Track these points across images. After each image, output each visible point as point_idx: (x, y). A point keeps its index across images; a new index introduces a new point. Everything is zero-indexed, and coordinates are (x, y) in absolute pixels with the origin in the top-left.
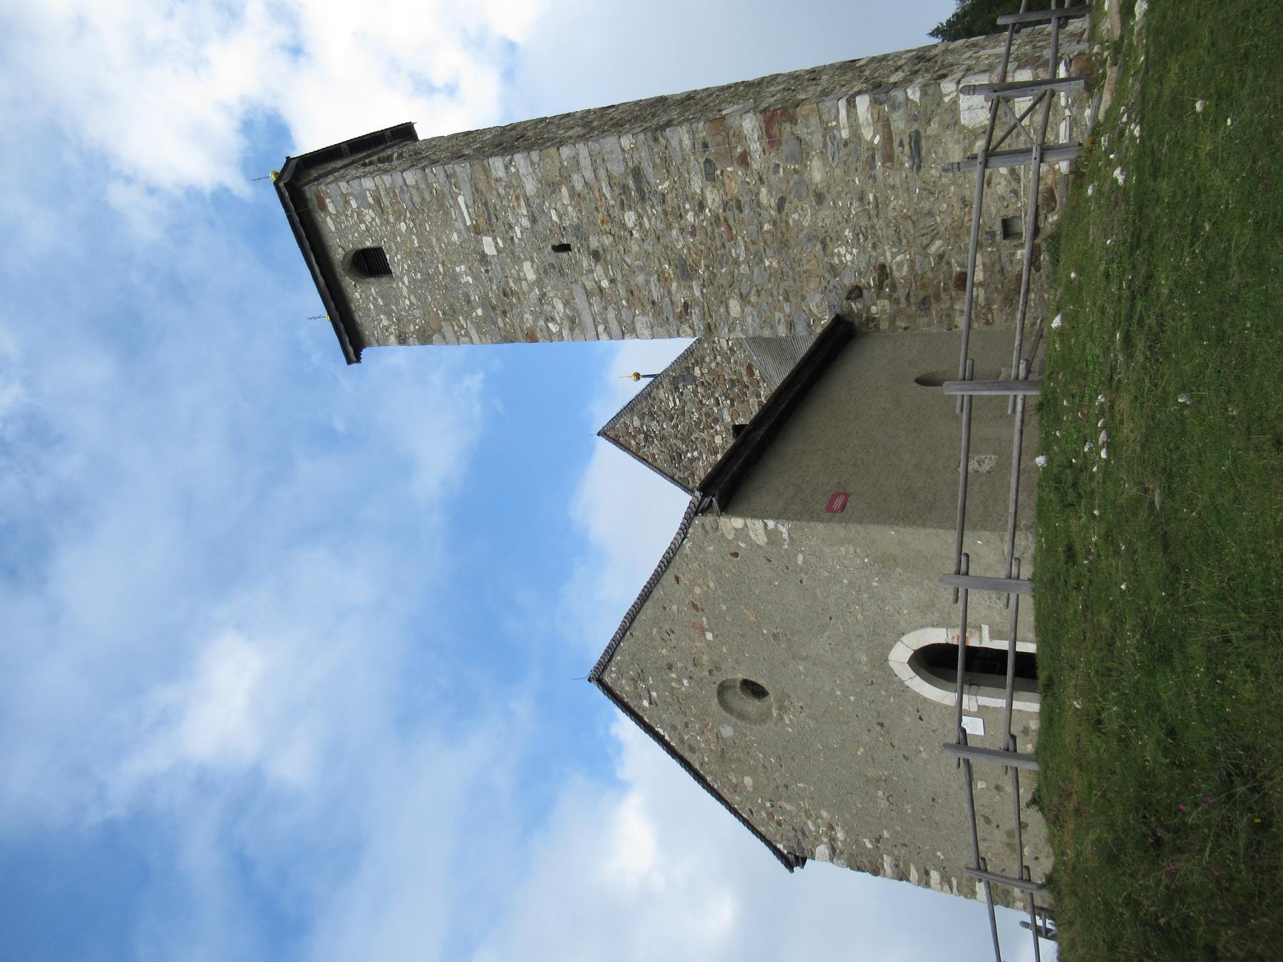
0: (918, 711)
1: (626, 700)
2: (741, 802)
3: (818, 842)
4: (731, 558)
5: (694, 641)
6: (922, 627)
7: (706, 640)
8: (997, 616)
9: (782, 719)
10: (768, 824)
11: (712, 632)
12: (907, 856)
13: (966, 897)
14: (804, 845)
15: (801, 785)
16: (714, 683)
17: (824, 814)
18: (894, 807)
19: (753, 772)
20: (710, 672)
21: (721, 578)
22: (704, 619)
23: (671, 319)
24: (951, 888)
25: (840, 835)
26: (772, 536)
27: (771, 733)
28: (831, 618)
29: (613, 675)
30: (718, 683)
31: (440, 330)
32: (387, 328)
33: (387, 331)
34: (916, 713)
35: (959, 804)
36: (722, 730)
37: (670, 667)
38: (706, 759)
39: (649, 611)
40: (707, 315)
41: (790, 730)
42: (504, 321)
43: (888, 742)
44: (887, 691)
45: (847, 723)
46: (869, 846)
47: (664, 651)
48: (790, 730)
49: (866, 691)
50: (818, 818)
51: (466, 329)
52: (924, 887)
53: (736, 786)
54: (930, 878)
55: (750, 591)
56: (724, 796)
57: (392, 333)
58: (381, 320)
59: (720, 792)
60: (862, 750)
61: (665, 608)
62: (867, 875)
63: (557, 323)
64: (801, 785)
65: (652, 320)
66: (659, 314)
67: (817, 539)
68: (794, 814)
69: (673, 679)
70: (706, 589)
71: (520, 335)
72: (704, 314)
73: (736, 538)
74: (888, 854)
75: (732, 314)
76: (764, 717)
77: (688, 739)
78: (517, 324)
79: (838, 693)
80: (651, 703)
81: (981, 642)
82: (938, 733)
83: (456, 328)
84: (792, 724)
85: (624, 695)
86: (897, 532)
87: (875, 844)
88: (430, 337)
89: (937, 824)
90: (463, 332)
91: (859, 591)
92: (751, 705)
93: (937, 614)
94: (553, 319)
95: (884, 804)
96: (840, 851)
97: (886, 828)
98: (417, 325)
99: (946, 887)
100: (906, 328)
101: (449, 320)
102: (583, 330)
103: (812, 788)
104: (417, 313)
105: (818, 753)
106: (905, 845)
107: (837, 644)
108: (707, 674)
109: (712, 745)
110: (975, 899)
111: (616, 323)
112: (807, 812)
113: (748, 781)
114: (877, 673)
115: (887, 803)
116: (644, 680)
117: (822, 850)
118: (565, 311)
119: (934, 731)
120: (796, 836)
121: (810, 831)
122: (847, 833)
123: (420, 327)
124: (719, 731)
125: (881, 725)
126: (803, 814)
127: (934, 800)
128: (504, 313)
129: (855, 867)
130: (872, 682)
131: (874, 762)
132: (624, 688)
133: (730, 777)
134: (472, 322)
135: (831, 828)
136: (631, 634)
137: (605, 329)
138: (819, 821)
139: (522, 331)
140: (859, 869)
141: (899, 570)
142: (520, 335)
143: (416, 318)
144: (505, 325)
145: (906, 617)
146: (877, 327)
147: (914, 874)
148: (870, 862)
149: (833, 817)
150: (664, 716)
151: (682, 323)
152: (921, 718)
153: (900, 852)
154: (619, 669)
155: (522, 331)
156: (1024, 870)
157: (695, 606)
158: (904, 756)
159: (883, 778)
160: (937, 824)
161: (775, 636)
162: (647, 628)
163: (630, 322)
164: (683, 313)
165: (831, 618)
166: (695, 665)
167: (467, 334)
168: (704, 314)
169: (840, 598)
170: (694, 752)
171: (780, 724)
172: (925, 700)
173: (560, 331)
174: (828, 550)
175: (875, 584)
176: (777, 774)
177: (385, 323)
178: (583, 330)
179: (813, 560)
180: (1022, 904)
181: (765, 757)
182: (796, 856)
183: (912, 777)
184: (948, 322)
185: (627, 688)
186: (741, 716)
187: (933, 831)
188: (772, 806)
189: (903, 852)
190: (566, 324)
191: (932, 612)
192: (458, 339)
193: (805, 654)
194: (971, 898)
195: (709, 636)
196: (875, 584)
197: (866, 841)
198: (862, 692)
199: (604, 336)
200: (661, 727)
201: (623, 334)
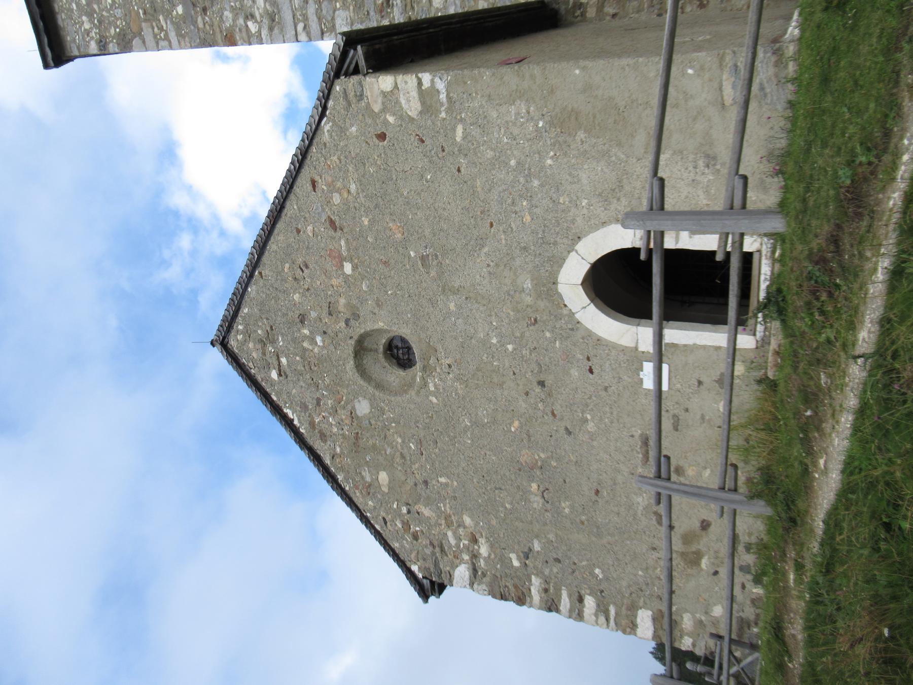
0: (588, 359)
1: (253, 371)
2: (375, 508)
3: (458, 561)
4: (377, 141)
5: (330, 278)
6: (604, 224)
7: (344, 274)
8: (702, 196)
9: (426, 385)
10: (403, 538)
11: (351, 261)
12: (560, 576)
13: (624, 632)
14: (441, 567)
15: (443, 480)
16: (351, 338)
17: (467, 520)
18: (549, 506)
19: (389, 467)
20: (347, 322)
21: (363, 176)
22: (343, 243)
23: (372, 13)
24: (607, 620)
25: (484, 550)
26: (427, 96)
27: (412, 406)
28: (492, 225)
29: (240, 337)
30: (356, 337)
31: (139, 34)
32: (88, 32)
33: (88, 35)
34: (586, 361)
35: (627, 497)
36: (357, 406)
37: (302, 319)
38: (338, 450)
39: (281, 238)
40: (409, 7)
41: (434, 400)
42: (203, 19)
43: (548, 410)
44: (552, 332)
45: (501, 385)
46: (516, 563)
47: (296, 297)
48: (434, 400)
49: (527, 334)
50: (459, 526)
51: (166, 31)
52: (575, 619)
53: (370, 485)
54: (584, 606)
55: (397, 191)
56: (355, 500)
57: (92, 38)
58: (83, 23)
59: (352, 495)
60: (516, 424)
61: (298, 231)
62: (511, 604)
63: (256, 21)
64: (443, 480)
65: (352, 14)
66: (360, 8)
67: (482, 96)
68: (433, 521)
69: (305, 336)
70: (345, 195)
71: (219, 37)
72: (406, 6)
73: (384, 110)
74: (537, 575)
75: (434, 4)
76: (407, 386)
77: (319, 423)
78: (216, 23)
79: (494, 341)
80: (280, 375)
81: (677, 242)
82: (610, 390)
83: (156, 30)
84: (436, 394)
85: (251, 364)
86: (584, 69)
87: (524, 560)
88: (131, 41)
89: (598, 527)
90: (162, 35)
91: (529, 176)
92: (394, 376)
93: (624, 201)
94: (252, 16)
95: (537, 502)
96: (483, 573)
97: (537, 537)
98: (118, 27)
99: (602, 619)
100: (614, 16)
101: (149, 20)
102: (282, 30)
103: (455, 483)
104: (119, 12)
105: (465, 432)
106: (558, 560)
107: (497, 265)
108: (343, 324)
109: (346, 428)
110: (635, 635)
111: (315, 19)
112: (447, 518)
113: (383, 477)
114: (542, 304)
115: (541, 501)
116: (274, 342)
117: (462, 572)
118: (265, 5)
119: (606, 389)
120: (433, 554)
121: (450, 547)
122: (492, 546)
123: (121, 30)
124: (353, 407)
125: (542, 384)
126: (443, 522)
127: (597, 492)
128: (205, 10)
129: (498, 596)
130: (536, 320)
131: (530, 440)
132: (251, 354)
133: (363, 474)
134: (172, 22)
135: (475, 541)
136: (260, 273)
137: (305, 28)
138: (461, 530)
139: (221, 32)
140: (503, 597)
141: (581, 135)
142: (219, 37)
143: (117, 19)
144: (204, 24)
145: (585, 211)
146: (583, 14)
147: (565, 602)
148: (516, 586)
149: (477, 524)
150: (294, 391)
151: (382, 17)
152: (591, 371)
153: (551, 570)
154: (246, 326)
155: (221, 32)
156: (730, 470)
157: (332, 223)
158: (566, 429)
159: (539, 464)
160: (598, 527)
161: (424, 259)
162: (279, 263)
163: (330, 18)
164: (385, 5)
165: (492, 225)
166: (330, 314)
167: (167, 38)
168: (406, 6)
169: (504, 191)
170: (325, 441)
171: (423, 391)
172: (599, 339)
173: (259, 32)
174: (494, 114)
175: (549, 162)
176: (417, 465)
177: (87, 26)
178: (282, 30)
179: (475, 132)
180: (691, 640)
181: (403, 442)
182: (432, 583)
183: (574, 460)
184: (658, 7)
185: (254, 355)
186: (379, 386)
187: (594, 539)
188: (409, 512)
189: (555, 570)
190: (266, 21)
191: (618, 199)
192: (157, 43)
193: (457, 285)
194: (630, 633)
195: (348, 268)
196: (549, 162)
197: (513, 556)
198: (522, 335)
199: (303, 37)
200: (290, 408)
201: (323, 33)
